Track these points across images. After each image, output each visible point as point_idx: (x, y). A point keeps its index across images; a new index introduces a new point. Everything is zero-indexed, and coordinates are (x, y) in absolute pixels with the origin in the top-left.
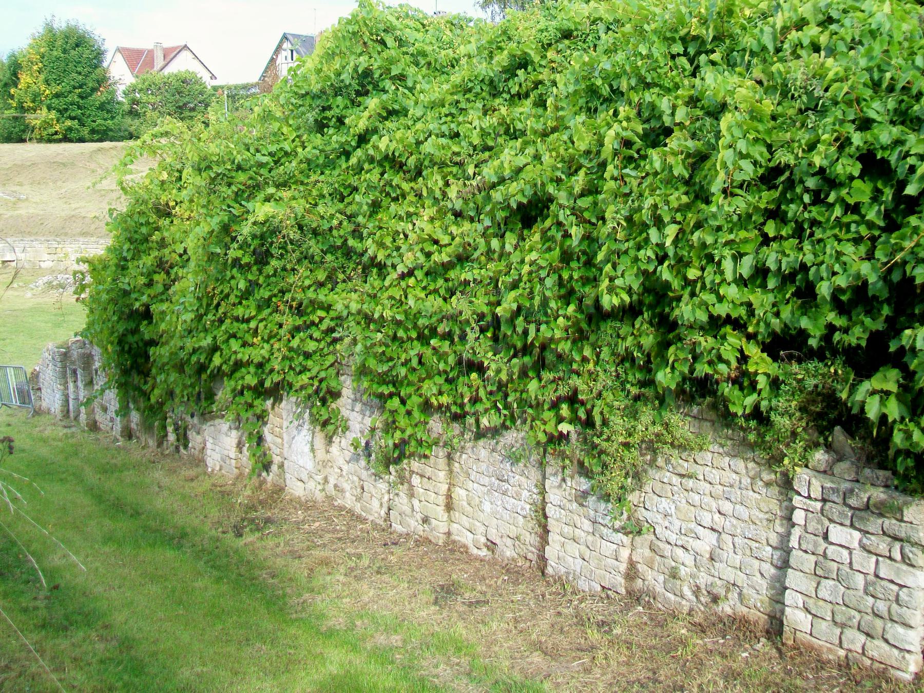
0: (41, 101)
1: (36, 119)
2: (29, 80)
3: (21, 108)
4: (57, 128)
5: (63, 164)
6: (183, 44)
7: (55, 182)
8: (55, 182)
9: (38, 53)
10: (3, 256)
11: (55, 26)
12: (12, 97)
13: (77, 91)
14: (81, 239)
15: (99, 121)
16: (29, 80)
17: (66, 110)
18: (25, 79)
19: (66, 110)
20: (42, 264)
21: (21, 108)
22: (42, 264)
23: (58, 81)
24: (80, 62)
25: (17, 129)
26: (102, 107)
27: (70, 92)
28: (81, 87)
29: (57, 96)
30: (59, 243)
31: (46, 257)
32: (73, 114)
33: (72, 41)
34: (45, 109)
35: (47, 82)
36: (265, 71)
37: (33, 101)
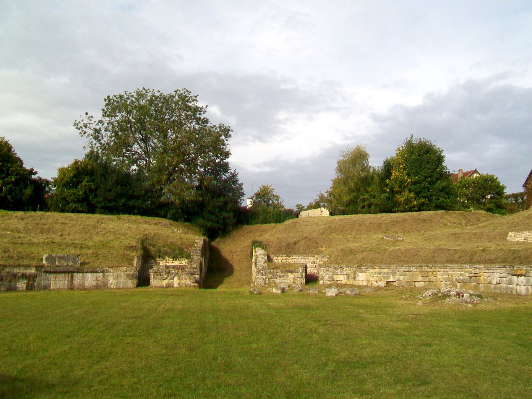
0: (405, 187)
1: (401, 198)
2: (397, 174)
3: (392, 191)
4: (415, 203)
5: (424, 220)
6: (474, 169)
7: (419, 231)
8: (419, 231)
9: (403, 158)
10: (387, 278)
11: (414, 142)
12: (387, 185)
13: (428, 179)
14: (310, 303)
15: (441, 199)
16: (397, 174)
17: (420, 192)
18: (395, 174)
19: (420, 192)
20: (416, 284)
21: (392, 191)
22: (416, 284)
23: (416, 173)
24: (428, 162)
25: (389, 205)
26: (443, 190)
27: (423, 180)
28: (430, 177)
29: (415, 183)
30: (431, 268)
31: (420, 278)
32: (425, 195)
33: (424, 149)
34: (407, 192)
35: (408, 174)
36: (527, 181)
37: (400, 187)
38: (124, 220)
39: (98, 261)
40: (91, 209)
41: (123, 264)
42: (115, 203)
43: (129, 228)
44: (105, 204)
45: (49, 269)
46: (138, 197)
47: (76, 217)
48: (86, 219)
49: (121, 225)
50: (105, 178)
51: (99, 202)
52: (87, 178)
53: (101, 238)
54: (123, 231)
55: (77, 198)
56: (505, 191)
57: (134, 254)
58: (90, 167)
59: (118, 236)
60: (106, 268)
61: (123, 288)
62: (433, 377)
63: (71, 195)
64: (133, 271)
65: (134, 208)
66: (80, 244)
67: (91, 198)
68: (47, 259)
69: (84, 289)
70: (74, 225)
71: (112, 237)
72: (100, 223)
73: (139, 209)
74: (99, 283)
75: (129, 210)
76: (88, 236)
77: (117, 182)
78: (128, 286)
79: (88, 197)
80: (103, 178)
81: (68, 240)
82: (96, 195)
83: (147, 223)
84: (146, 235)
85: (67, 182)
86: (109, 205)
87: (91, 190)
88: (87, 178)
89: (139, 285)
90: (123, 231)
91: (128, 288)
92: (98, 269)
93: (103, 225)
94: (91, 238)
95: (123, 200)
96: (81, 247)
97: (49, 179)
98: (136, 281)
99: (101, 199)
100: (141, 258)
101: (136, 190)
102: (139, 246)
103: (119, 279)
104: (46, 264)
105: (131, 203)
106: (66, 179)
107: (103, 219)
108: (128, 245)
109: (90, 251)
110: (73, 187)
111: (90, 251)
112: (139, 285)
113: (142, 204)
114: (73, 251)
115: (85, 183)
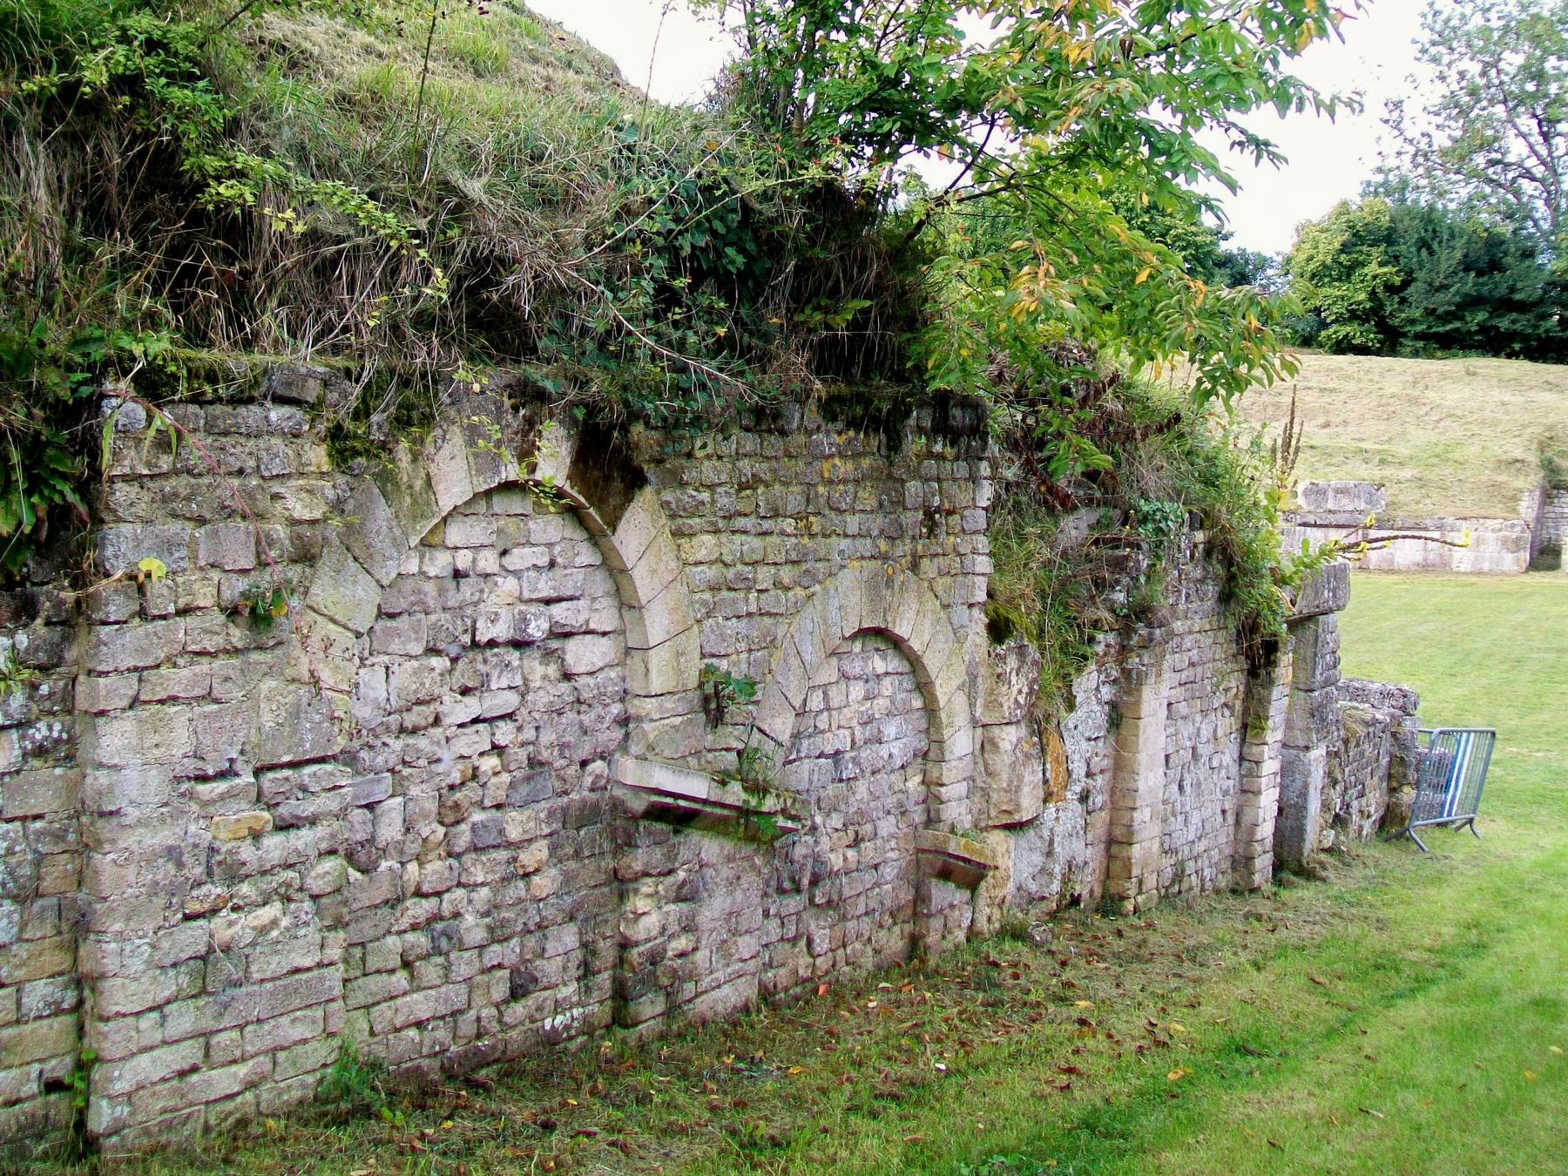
38: (1486, 378)
39: (1428, 501)
40: (1390, 341)
41: (1491, 512)
42: (1457, 324)
43: (1503, 404)
44: (1430, 327)
45: (1311, 519)
46: (1522, 307)
47: (1354, 368)
48: (1381, 375)
49: (1480, 393)
50: (1431, 253)
51: (1413, 322)
52: (1377, 253)
53: (1432, 437)
54: (1487, 413)
55: (1352, 312)
56: (1259, 829)
57: (1520, 483)
58: (1385, 220)
59: (1476, 429)
60: (1450, 520)
61: (1490, 573)
62: (1074, 533)
63: (1334, 303)
64: (1518, 529)
65: (1512, 336)
66: (1379, 452)
67: (1389, 309)
68: (1306, 493)
69: (1391, 571)
70: (1353, 396)
71: (1457, 432)
72: (1420, 386)
73: (1525, 338)
74: (1431, 556)
75: (1495, 344)
76: (1395, 428)
77: (1467, 265)
78: (1505, 569)
79: (1381, 306)
80: (1424, 252)
81: (1345, 439)
82: (1403, 301)
83: (1551, 386)
84: (1550, 428)
85: (1324, 265)
86: (1441, 329)
87: (1390, 288)
88: (1377, 253)
89: (1533, 566)
90: (1487, 413)
91: (1503, 573)
92: (1428, 522)
93: (1430, 394)
94: (1404, 434)
95: (1481, 316)
96: (1382, 461)
97: (1268, 253)
98: (1525, 556)
99: (1417, 314)
100: (1537, 493)
101: (1519, 285)
102: (1533, 458)
103: (1482, 548)
104: (1304, 505)
105: (1504, 324)
106: (1320, 257)
107: (1428, 373)
108: (1504, 457)
109: (1406, 473)
110: (1340, 279)
111: (1406, 473)
112: (1533, 566)
113: (1536, 327)
114: (1371, 472)
115: (1373, 268)
